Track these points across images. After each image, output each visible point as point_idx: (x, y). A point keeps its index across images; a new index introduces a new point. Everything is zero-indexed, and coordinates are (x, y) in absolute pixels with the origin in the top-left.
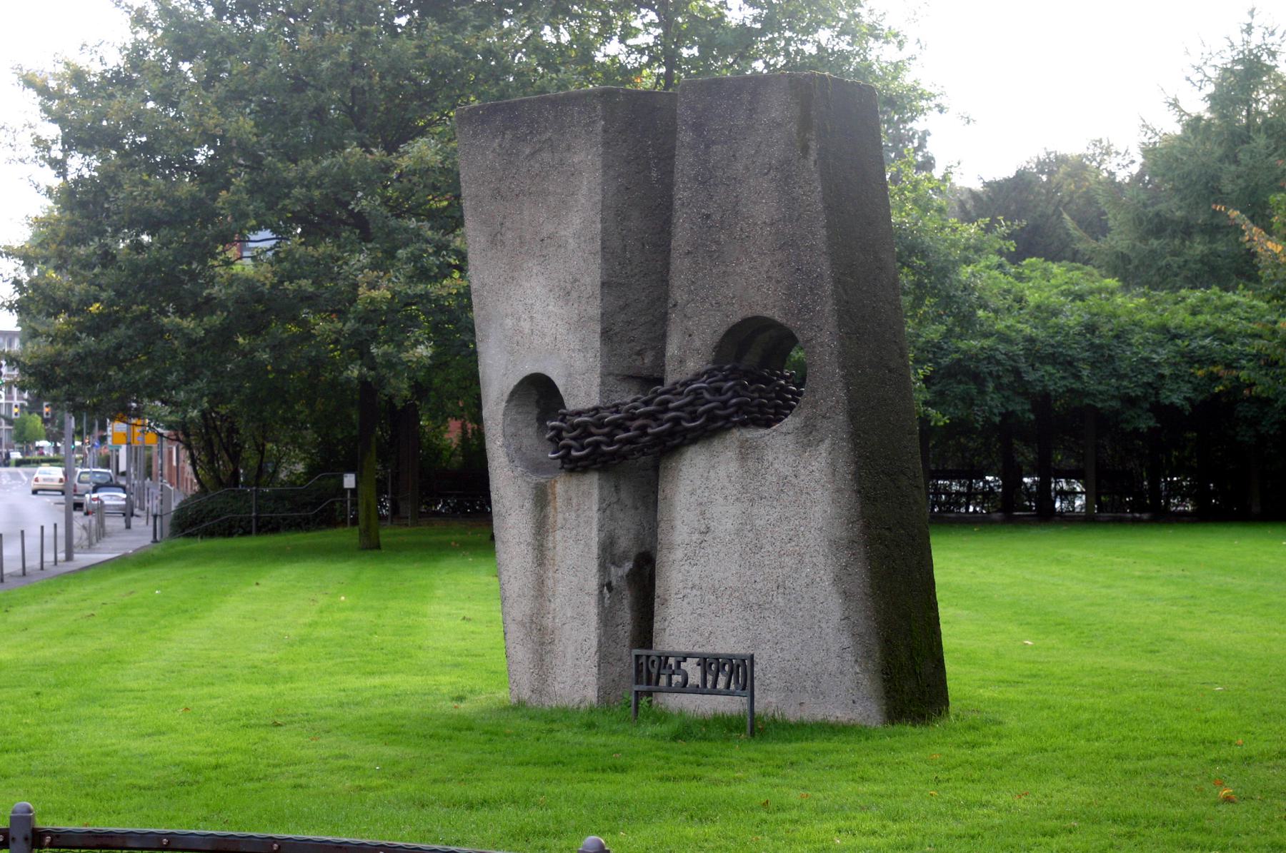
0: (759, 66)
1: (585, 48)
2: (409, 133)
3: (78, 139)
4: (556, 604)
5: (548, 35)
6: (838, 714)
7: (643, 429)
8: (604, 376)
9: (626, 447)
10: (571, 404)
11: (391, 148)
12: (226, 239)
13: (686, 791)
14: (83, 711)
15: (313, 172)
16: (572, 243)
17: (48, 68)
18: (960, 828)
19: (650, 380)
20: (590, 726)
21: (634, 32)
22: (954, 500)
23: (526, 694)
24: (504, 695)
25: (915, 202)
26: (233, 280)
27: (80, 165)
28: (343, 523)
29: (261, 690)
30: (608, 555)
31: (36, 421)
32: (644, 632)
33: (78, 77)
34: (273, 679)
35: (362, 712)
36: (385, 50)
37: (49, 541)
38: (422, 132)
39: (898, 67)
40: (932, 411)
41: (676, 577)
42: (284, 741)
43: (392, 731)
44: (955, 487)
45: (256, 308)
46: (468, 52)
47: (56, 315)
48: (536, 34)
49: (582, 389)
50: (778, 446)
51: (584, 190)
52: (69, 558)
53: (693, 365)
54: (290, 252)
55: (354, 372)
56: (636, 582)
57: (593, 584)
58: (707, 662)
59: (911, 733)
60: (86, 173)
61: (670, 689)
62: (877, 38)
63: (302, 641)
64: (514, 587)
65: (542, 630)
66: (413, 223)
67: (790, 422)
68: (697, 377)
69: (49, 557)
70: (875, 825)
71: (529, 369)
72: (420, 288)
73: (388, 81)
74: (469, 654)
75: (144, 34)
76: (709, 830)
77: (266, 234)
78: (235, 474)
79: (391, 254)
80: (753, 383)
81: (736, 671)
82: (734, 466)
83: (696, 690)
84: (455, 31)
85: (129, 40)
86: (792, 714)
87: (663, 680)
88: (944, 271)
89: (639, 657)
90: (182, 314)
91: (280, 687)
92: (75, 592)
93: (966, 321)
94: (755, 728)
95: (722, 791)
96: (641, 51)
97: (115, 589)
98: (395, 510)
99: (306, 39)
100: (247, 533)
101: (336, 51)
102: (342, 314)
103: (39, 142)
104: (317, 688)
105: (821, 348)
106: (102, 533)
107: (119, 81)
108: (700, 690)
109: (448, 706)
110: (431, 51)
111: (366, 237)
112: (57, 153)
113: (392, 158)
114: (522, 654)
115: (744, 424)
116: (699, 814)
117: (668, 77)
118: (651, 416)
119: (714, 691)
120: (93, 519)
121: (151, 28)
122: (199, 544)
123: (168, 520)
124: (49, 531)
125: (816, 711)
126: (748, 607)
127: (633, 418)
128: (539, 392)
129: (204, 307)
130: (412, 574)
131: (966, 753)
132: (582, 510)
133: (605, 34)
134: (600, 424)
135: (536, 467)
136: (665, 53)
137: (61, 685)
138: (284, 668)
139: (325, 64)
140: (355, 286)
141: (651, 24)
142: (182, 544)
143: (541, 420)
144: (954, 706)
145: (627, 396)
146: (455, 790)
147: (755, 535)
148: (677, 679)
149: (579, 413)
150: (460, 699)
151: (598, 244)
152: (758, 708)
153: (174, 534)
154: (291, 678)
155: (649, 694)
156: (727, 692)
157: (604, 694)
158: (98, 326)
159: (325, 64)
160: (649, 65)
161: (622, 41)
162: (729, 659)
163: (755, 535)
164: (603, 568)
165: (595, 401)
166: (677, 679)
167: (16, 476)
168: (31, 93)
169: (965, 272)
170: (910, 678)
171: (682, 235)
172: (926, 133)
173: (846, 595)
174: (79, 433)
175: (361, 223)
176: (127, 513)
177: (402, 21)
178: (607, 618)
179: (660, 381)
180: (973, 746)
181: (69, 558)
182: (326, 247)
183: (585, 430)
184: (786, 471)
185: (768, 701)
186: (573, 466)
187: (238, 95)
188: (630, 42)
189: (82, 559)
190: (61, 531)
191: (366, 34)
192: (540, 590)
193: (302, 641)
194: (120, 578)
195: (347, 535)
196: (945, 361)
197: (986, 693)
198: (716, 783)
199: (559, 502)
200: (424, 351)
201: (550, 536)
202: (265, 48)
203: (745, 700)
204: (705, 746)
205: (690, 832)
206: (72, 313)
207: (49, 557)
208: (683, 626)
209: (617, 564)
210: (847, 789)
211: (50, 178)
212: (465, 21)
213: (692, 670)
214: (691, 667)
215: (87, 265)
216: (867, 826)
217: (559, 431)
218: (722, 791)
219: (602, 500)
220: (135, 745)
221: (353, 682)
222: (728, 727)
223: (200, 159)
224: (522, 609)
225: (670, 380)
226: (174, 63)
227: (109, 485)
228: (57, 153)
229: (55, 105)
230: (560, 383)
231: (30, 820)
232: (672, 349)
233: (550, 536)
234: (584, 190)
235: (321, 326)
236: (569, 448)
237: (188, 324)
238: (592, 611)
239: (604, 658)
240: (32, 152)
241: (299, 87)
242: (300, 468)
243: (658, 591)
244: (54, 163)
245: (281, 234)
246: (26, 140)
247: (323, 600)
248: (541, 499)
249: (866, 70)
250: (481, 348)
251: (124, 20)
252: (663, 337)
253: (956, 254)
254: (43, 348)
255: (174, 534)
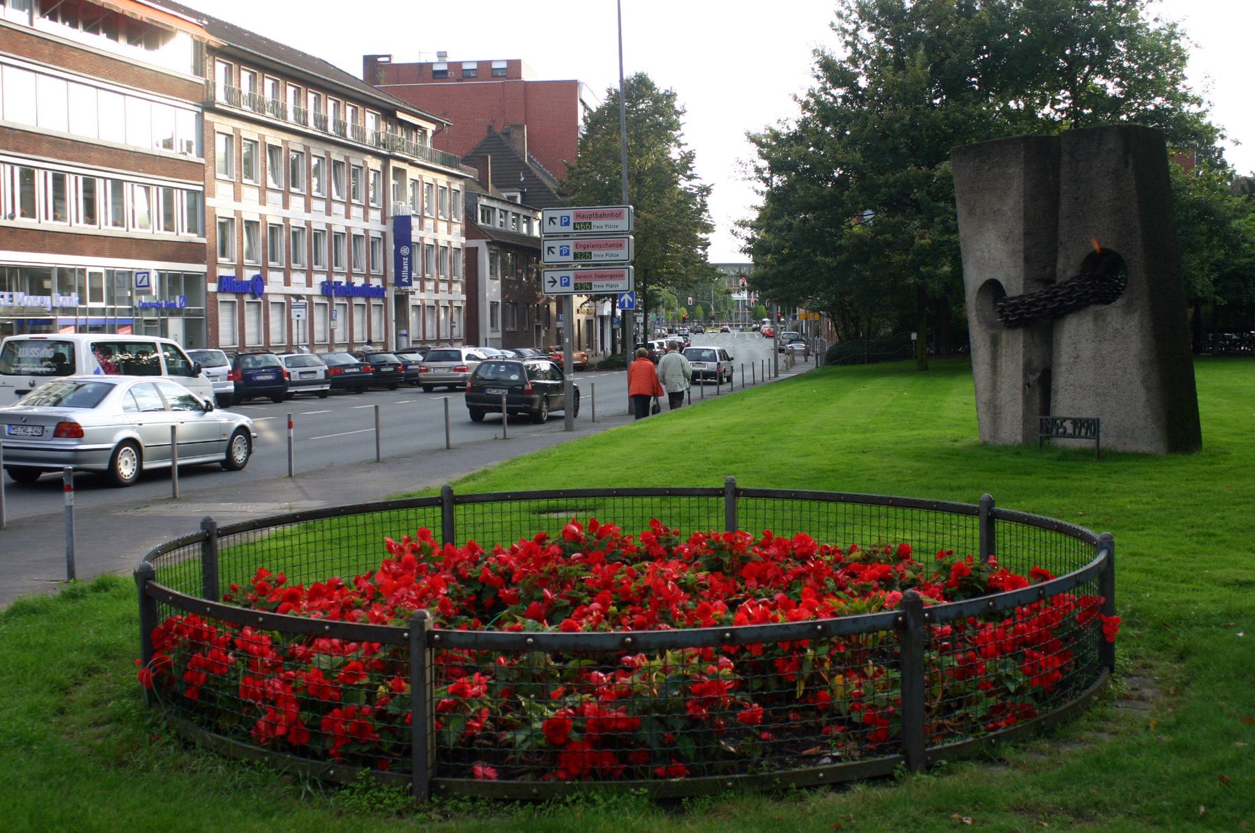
0: (1124, 117)
1: (1030, 111)
2: (942, 157)
3: (776, 168)
4: (1002, 393)
5: (1012, 104)
6: (1143, 448)
7: (1045, 306)
8: (1025, 279)
9: (1035, 316)
10: (1009, 294)
11: (931, 166)
12: (849, 214)
13: (1060, 484)
14: (773, 445)
15: (891, 180)
16: (1009, 213)
17: (760, 130)
18: (1191, 501)
19: (1048, 281)
20: (1018, 454)
21: (1059, 102)
22: (1234, 343)
23: (987, 438)
24: (976, 438)
25: (1208, 186)
26: (852, 235)
27: (777, 180)
28: (910, 357)
29: (859, 436)
30: (1028, 369)
31: (762, 309)
32: (1046, 407)
33: (776, 136)
34: (866, 431)
35: (906, 446)
36: (928, 117)
37: (766, 368)
38: (947, 158)
39: (1201, 115)
40: (1218, 298)
41: (1063, 380)
42: (866, 459)
43: (919, 456)
44: (1234, 337)
45: (864, 249)
46: (970, 116)
47: (766, 254)
48: (1007, 106)
49: (1014, 287)
50: (1114, 315)
51: (1015, 186)
52: (776, 375)
53: (1070, 273)
54: (880, 221)
55: (911, 281)
56: (1041, 383)
57: (1020, 384)
58: (1077, 423)
59: (1182, 458)
60: (780, 184)
61: (1058, 435)
62: (1186, 101)
63: (883, 413)
64: (981, 386)
65: (995, 407)
66: (942, 204)
67: (1120, 302)
68: (1072, 279)
69: (766, 375)
70: (1150, 500)
71: (988, 276)
72: (946, 237)
73: (930, 132)
74: (964, 420)
75: (808, 114)
76: (1066, 501)
77: (869, 212)
78: (857, 334)
79: (931, 220)
80: (1100, 283)
81: (1090, 426)
82: (1091, 325)
83: (1071, 436)
84: (963, 105)
85: (801, 117)
86: (1120, 448)
87: (1054, 431)
88: (1224, 222)
89: (1043, 421)
90: (826, 255)
91: (868, 435)
92: (775, 391)
93: (1236, 248)
94: (1100, 455)
95: (1076, 484)
96: (1062, 111)
97: (795, 390)
98: (937, 351)
99: (886, 113)
100: (863, 363)
101: (903, 118)
102: (906, 251)
103: (758, 170)
104: (885, 437)
105: (1136, 260)
106: (793, 363)
107: (796, 138)
108: (1073, 436)
109: (948, 444)
110: (951, 116)
111: (919, 211)
112: (767, 175)
113: (932, 172)
114: (986, 419)
115: (1096, 303)
116: (1063, 493)
117: (1076, 124)
118: (1049, 299)
119: (1080, 437)
120: (789, 358)
121: (812, 110)
122: (839, 368)
123: (824, 356)
124: (766, 363)
125: (1132, 447)
126: (1098, 395)
127: (1039, 300)
128: (993, 288)
129: (838, 250)
130: (943, 382)
131: (1207, 468)
132: (1015, 348)
133: (1043, 104)
134: (1023, 303)
135: (991, 325)
136: (1072, 113)
137: (764, 433)
138: (871, 426)
139: (897, 125)
140: (913, 238)
141: (1066, 98)
142: (830, 368)
143: (995, 302)
144: (1204, 446)
145: (1037, 289)
146: (946, 482)
147: (1101, 361)
148: (1061, 430)
149: (1013, 298)
150: (956, 441)
151: (1022, 214)
152: (1103, 444)
153: (827, 363)
154: (874, 431)
155: (1048, 438)
156: (1086, 437)
157: (1025, 437)
158: (783, 261)
159: (897, 125)
160: (1066, 118)
161: (1052, 107)
162: (1087, 420)
163: (1101, 361)
164: (1025, 376)
165: (1021, 292)
166: (1061, 430)
167: (752, 336)
168: (754, 145)
169: (1235, 224)
170: (1180, 428)
171: (1065, 206)
172: (1222, 149)
173: (1147, 388)
174: (783, 315)
175: (917, 205)
176: (806, 354)
177: (937, 101)
178: (1027, 401)
179: (1054, 282)
180: (1211, 464)
181: (776, 375)
182: (899, 218)
183: (1016, 306)
184: (1119, 326)
185: (1107, 441)
186: (1010, 325)
187: (853, 142)
188: (1057, 107)
189: (782, 376)
190: (772, 362)
191: (918, 109)
192: (994, 387)
193: (883, 413)
194: (798, 385)
195: (912, 364)
196: (1226, 270)
197: (1225, 439)
198: (1075, 480)
199: (1003, 343)
200: (947, 269)
201: (999, 362)
202: (867, 118)
203: (1094, 441)
204: (1073, 463)
205: (1056, 502)
206: (774, 253)
207: (766, 375)
208: (1066, 404)
209: (1033, 374)
210: (1140, 483)
211: (762, 187)
212: (969, 100)
213: (1068, 425)
214: (1068, 424)
215: (781, 230)
216: (1145, 500)
217: (1003, 307)
218: (1076, 484)
219: (1025, 342)
220: (796, 460)
221: (904, 433)
222: (1085, 454)
223: (836, 175)
224: (985, 396)
225: (1059, 281)
226: (823, 128)
227: (797, 340)
228: (767, 175)
229: (765, 151)
230: (1003, 283)
231: (734, 484)
232: (1060, 266)
233: (999, 362)
234: (1015, 186)
235: (897, 258)
236: (1008, 316)
237: (829, 260)
238: (1020, 397)
239: (1026, 420)
240: (754, 174)
241: (885, 137)
242: (890, 330)
243: (1053, 387)
244: (765, 180)
245: (876, 211)
246: (751, 168)
247: (895, 394)
248: (995, 342)
249: (1182, 117)
250: (964, 267)
251: (798, 107)
252: (1055, 260)
253: (1229, 214)
254: (761, 270)
255: (827, 363)
